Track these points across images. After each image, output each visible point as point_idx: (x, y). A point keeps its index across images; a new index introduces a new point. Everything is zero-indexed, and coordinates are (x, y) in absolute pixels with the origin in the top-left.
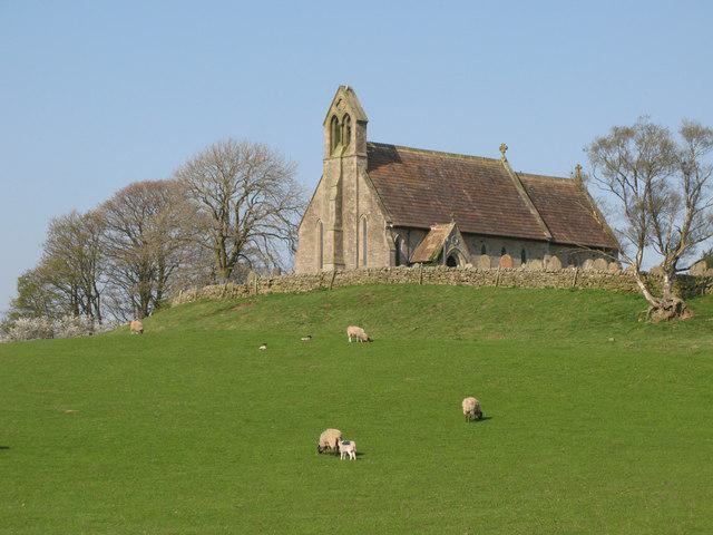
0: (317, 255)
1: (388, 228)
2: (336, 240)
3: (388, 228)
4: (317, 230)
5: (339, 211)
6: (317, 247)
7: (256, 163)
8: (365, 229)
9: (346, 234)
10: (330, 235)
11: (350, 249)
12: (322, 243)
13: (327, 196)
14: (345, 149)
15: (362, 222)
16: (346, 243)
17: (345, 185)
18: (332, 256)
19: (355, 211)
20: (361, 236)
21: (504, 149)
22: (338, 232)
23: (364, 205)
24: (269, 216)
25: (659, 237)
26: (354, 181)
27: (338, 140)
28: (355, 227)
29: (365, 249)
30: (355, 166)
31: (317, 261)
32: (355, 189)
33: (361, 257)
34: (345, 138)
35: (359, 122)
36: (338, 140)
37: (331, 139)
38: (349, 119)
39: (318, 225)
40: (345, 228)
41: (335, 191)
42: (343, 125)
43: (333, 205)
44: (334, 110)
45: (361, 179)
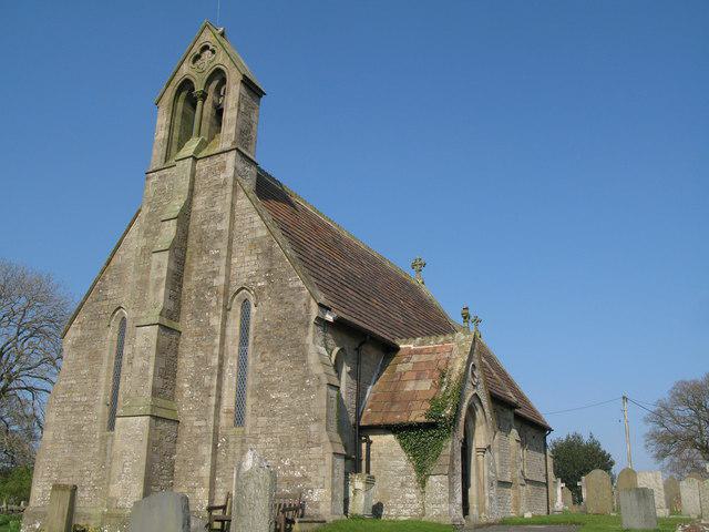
0: (103, 395)
1: (320, 321)
2: (160, 351)
3: (320, 321)
4: (111, 334)
5: (176, 279)
6: (105, 379)
7: (33, 300)
8: (245, 329)
9: (188, 340)
10: (145, 339)
11: (196, 383)
12: (118, 366)
13: (148, 252)
14: (203, 145)
15: (236, 308)
16: (187, 363)
17: (196, 221)
18: (148, 394)
19: (219, 281)
20: (233, 348)
21: (419, 265)
22: (169, 328)
23: (247, 266)
24: (43, 366)
25: (216, 427)
26: (222, 207)
27: (186, 136)
28: (216, 322)
29: (242, 380)
30: (230, 172)
31: (101, 410)
32: (224, 226)
33: (229, 401)
34: (206, 126)
35: (247, 82)
36: (188, 119)
37: (171, 128)
38: (223, 81)
39: (115, 324)
40: (187, 324)
41: (170, 231)
42: (204, 96)
43: (161, 264)
44: (186, 69)
45: (244, 202)
